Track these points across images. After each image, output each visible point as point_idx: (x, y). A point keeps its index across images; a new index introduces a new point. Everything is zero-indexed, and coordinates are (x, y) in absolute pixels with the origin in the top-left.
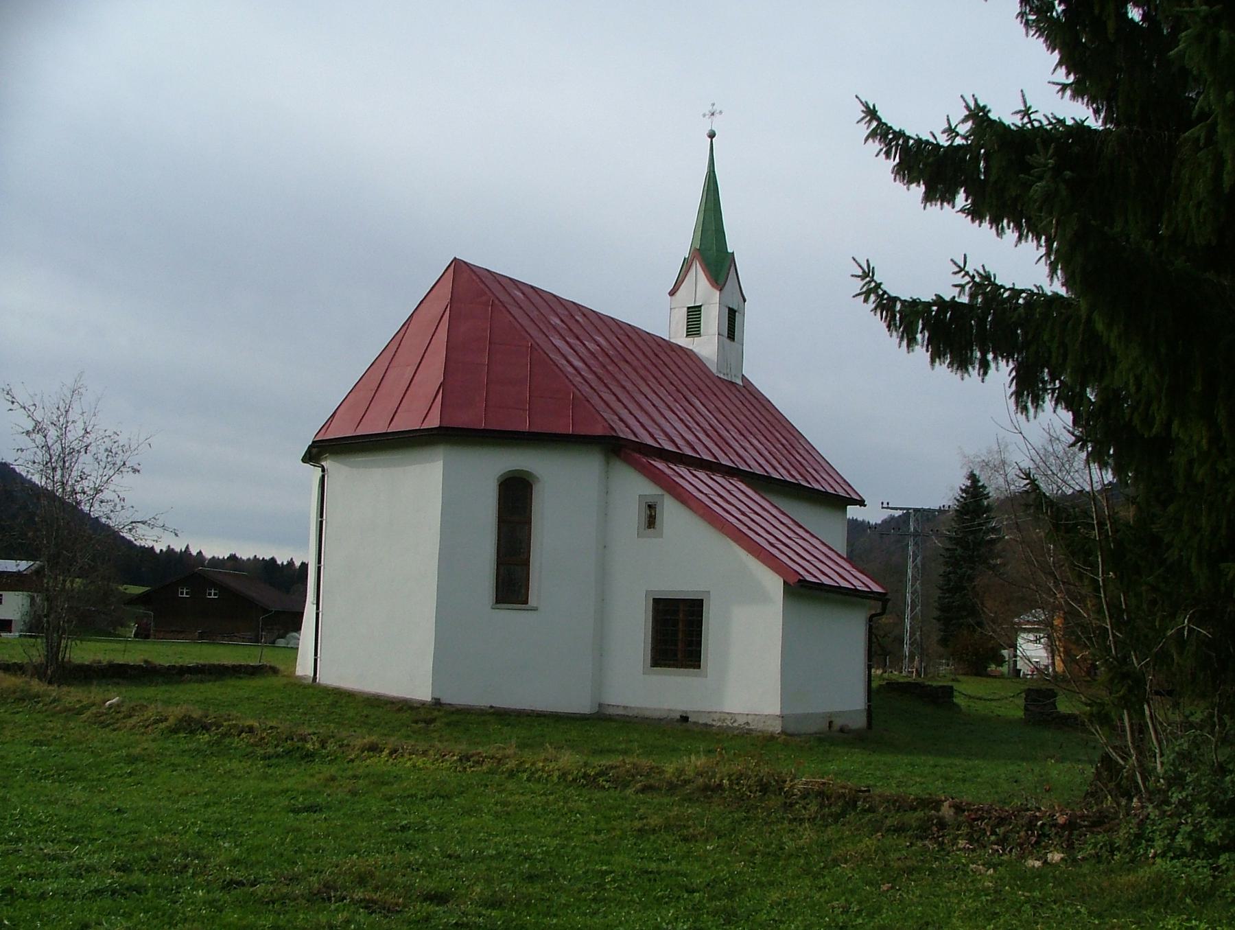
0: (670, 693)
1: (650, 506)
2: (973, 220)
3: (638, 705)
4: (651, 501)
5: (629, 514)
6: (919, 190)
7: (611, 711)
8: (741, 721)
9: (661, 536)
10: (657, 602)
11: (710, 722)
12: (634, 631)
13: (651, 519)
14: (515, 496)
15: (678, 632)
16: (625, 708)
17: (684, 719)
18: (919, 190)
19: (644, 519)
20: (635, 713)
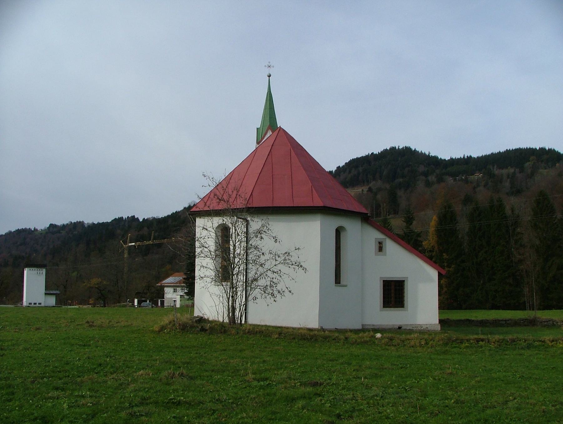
0: (393, 318)
1: (380, 243)
2: (470, 156)
3: (378, 324)
4: (380, 241)
5: (372, 246)
6: (136, 217)
7: (367, 327)
8: (424, 327)
9: (376, 254)
10: (404, 281)
11: (411, 328)
12: (376, 294)
13: (380, 248)
14: (339, 232)
15: (394, 293)
16: (373, 325)
17: (400, 328)
18: (136, 217)
19: (377, 248)
20: (378, 327)
